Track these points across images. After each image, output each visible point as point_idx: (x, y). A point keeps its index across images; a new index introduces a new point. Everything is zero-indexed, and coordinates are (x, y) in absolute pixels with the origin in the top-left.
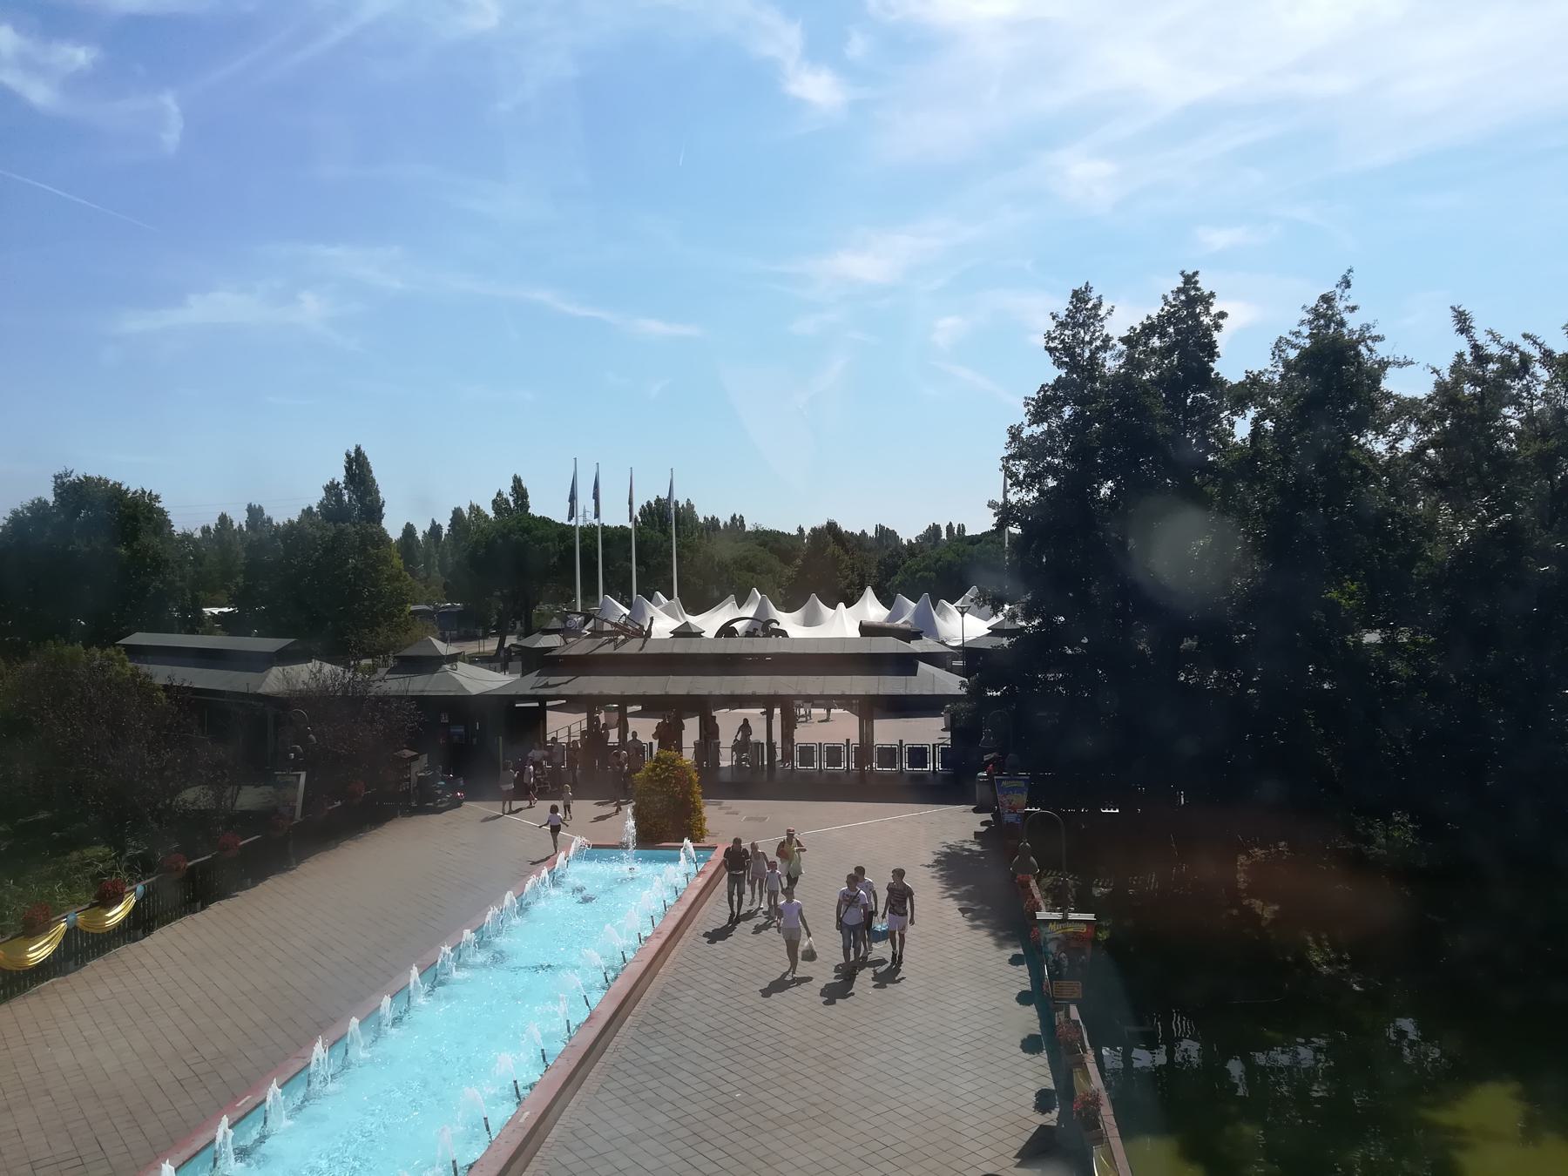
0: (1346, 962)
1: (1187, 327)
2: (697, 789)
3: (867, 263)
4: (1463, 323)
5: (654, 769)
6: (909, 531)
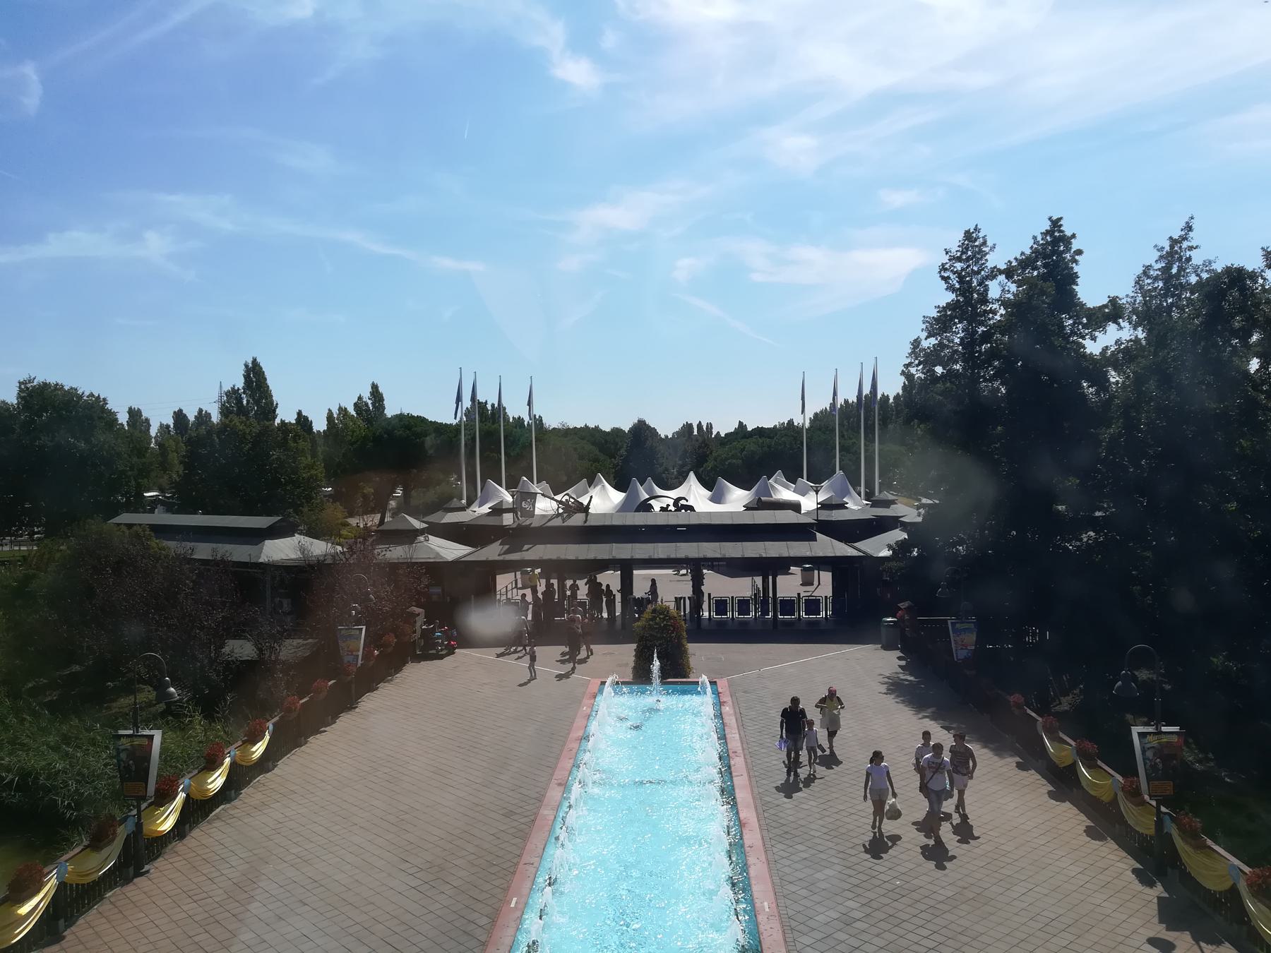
1: (1052, 261)
3: (621, 214)
5: (653, 619)
6: (606, 428)
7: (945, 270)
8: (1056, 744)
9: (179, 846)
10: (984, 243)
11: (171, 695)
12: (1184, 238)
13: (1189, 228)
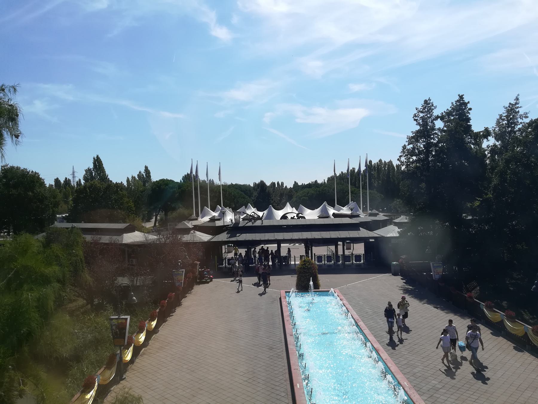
1: (460, 112)
3: (240, 94)
7: (415, 116)
8: (492, 313)
9: (133, 366)
10: (433, 105)
11: (134, 300)
12: (516, 104)
13: (517, 99)
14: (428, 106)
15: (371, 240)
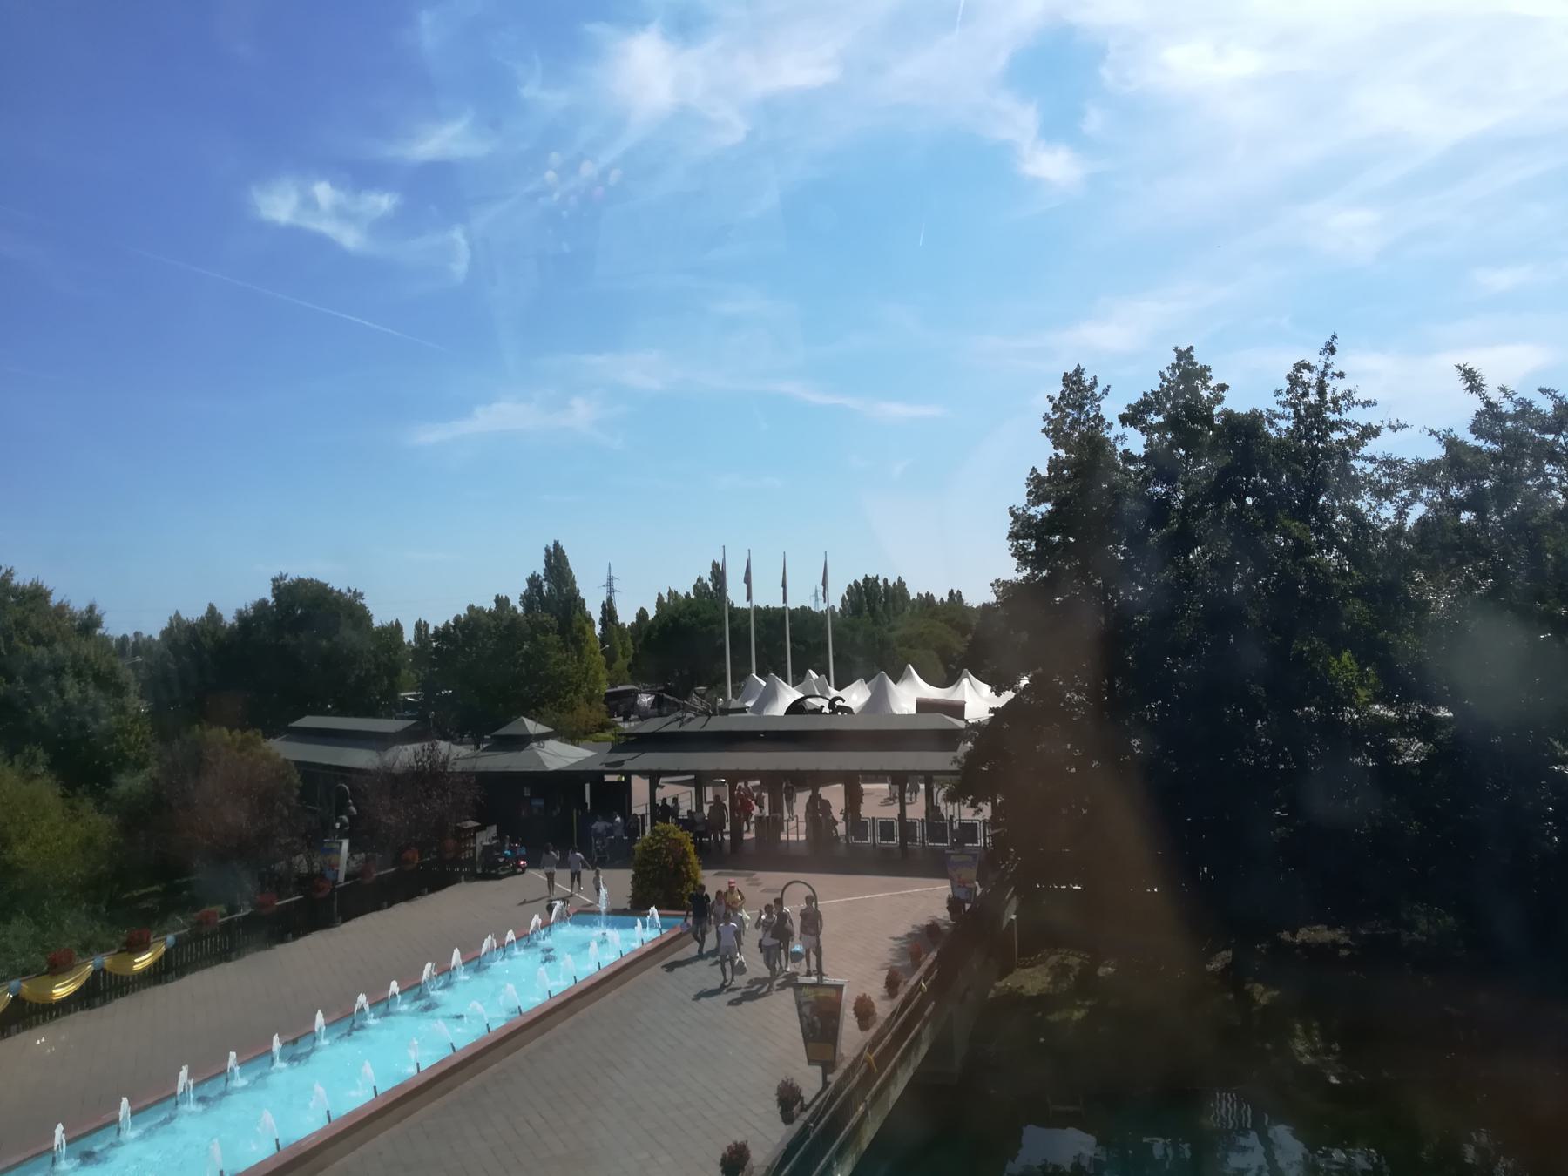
0: (1334, 1052)
2: (693, 858)
4: (1472, 380)
14: (1077, 391)
15: (608, 778)
